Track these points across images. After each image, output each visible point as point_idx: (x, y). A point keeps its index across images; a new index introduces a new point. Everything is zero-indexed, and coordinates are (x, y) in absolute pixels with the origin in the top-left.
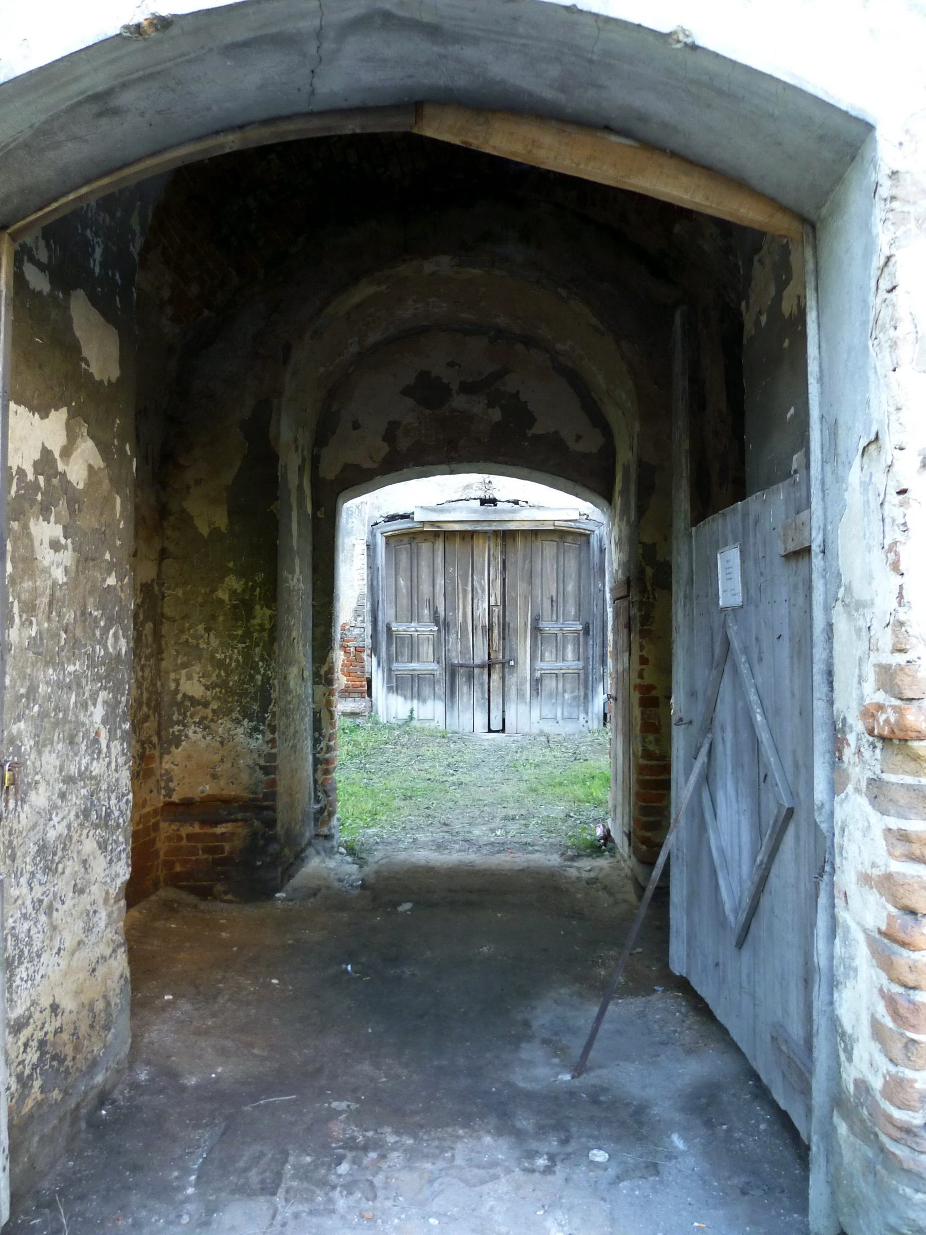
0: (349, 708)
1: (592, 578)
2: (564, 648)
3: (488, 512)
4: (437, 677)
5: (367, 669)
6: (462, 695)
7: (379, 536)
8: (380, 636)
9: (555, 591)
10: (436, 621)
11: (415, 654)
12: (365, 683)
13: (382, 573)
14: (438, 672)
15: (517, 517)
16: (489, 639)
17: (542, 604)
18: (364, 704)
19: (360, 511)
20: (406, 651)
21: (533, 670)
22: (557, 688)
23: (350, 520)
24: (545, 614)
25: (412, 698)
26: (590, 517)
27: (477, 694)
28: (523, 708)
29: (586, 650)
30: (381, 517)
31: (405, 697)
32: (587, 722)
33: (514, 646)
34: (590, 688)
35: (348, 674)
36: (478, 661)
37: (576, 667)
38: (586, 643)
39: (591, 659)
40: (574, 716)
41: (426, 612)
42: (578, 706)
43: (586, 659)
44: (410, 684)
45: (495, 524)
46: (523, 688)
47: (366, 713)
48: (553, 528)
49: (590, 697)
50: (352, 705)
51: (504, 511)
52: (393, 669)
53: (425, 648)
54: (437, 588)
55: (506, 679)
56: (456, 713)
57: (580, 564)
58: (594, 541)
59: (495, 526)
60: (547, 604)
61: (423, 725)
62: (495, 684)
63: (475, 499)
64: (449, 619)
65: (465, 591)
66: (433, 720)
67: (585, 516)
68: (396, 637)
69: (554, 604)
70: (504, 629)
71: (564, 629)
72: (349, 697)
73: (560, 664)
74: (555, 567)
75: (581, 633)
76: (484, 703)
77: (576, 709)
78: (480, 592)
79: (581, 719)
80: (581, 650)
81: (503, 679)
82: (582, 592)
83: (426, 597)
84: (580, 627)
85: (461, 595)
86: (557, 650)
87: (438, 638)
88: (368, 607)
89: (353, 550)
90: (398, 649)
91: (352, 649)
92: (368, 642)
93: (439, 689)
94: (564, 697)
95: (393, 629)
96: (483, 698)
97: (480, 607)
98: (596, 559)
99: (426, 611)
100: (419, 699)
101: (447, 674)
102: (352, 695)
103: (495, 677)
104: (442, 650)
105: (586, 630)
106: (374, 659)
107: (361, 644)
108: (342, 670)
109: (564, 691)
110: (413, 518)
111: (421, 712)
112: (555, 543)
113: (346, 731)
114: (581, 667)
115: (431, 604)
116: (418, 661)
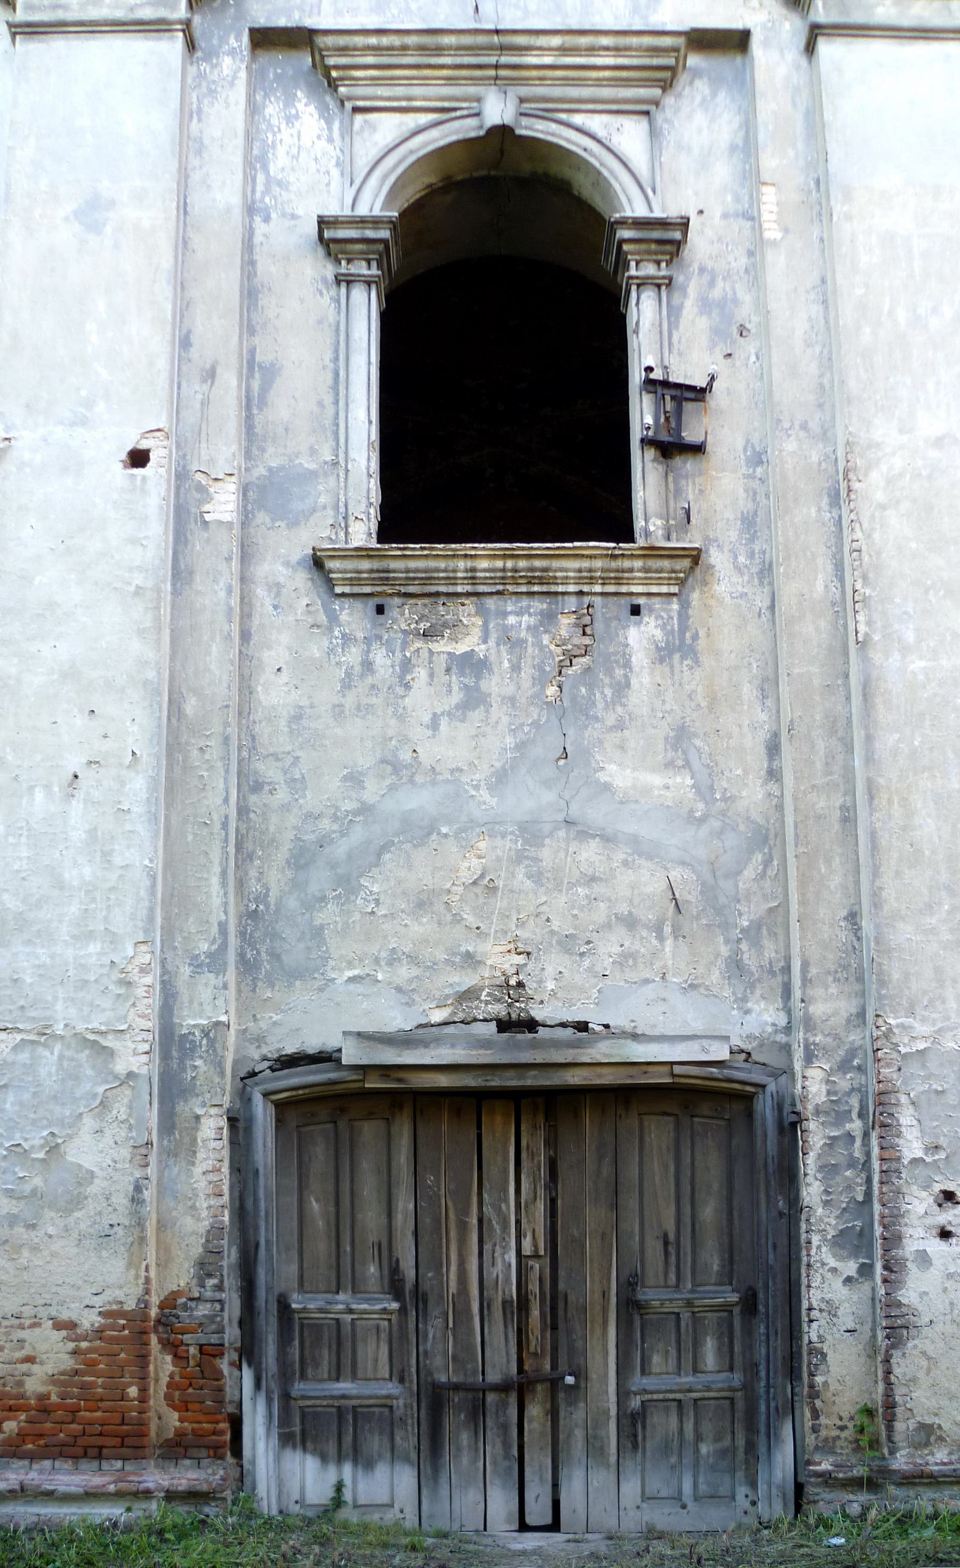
0: (184, 1481)
1: (762, 1187)
2: (697, 1345)
3: (518, 1046)
4: (399, 1413)
5: (230, 1392)
6: (459, 1449)
7: (258, 1099)
8: (261, 1321)
9: (672, 1222)
10: (395, 1287)
11: (347, 1361)
12: (224, 1426)
13: (267, 1181)
14: (401, 1402)
15: (588, 1055)
16: (520, 1331)
17: (642, 1252)
18: (221, 1472)
19: (212, 1043)
20: (325, 1356)
21: (623, 1394)
22: (681, 1431)
23: (188, 1063)
24: (650, 1272)
25: (340, 1460)
26: (755, 1057)
27: (494, 1448)
28: (602, 1478)
29: (749, 1347)
30: (265, 1059)
31: (324, 1458)
32: (754, 1503)
33: (579, 1344)
34: (763, 1429)
35: (183, 1407)
36: (493, 1377)
37: (725, 1385)
38: (748, 1332)
39: (762, 1367)
40: (724, 1490)
41: (372, 1269)
42: (733, 1471)
43: (751, 1368)
44: (334, 1428)
45: (533, 1073)
46: (602, 1433)
47: (228, 1494)
48: (668, 1080)
49: (762, 1450)
50: (192, 1475)
51: (556, 1044)
52: (294, 1394)
53: (371, 1348)
54: (399, 1218)
55: (562, 1414)
56: (444, 1492)
57: (730, 1162)
58: (765, 1107)
59: (535, 1077)
60: (654, 1249)
61: (367, 1518)
62: (535, 1425)
63: (485, 1020)
64: (426, 1286)
65: (463, 1227)
66: (392, 1506)
67: (743, 1056)
68: (302, 1326)
69: (671, 1249)
70: (554, 1309)
71: (697, 1303)
72: (185, 1457)
73: (687, 1379)
74: (672, 1168)
75: (737, 1310)
76: (510, 1468)
77: (727, 1478)
78: (497, 1228)
79: (740, 1497)
80: (737, 1348)
81: (554, 1414)
82: (736, 1222)
83: (372, 1238)
84: (734, 1298)
85: (453, 1234)
86: (679, 1350)
87: (400, 1327)
88: (231, 1257)
89: (197, 1129)
90: (307, 1352)
91: (193, 1350)
92: (232, 1334)
93: (404, 1439)
94: (697, 1451)
95: (294, 1306)
96: (507, 1456)
97: (499, 1262)
98: (771, 1144)
99: (372, 1269)
100: (355, 1462)
101: (423, 1405)
102: (193, 1452)
103: (535, 1411)
104: (409, 1353)
105: (750, 1304)
106: (247, 1375)
107: (214, 1339)
108: (168, 1397)
109: (699, 1438)
110: (338, 1061)
111: (361, 1486)
112: (671, 1119)
113: (167, 1536)
114: (737, 1383)
115: (385, 1253)
116: (354, 1377)
